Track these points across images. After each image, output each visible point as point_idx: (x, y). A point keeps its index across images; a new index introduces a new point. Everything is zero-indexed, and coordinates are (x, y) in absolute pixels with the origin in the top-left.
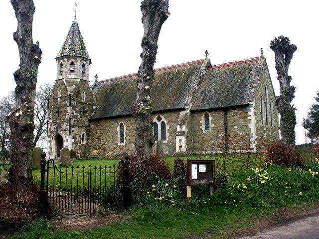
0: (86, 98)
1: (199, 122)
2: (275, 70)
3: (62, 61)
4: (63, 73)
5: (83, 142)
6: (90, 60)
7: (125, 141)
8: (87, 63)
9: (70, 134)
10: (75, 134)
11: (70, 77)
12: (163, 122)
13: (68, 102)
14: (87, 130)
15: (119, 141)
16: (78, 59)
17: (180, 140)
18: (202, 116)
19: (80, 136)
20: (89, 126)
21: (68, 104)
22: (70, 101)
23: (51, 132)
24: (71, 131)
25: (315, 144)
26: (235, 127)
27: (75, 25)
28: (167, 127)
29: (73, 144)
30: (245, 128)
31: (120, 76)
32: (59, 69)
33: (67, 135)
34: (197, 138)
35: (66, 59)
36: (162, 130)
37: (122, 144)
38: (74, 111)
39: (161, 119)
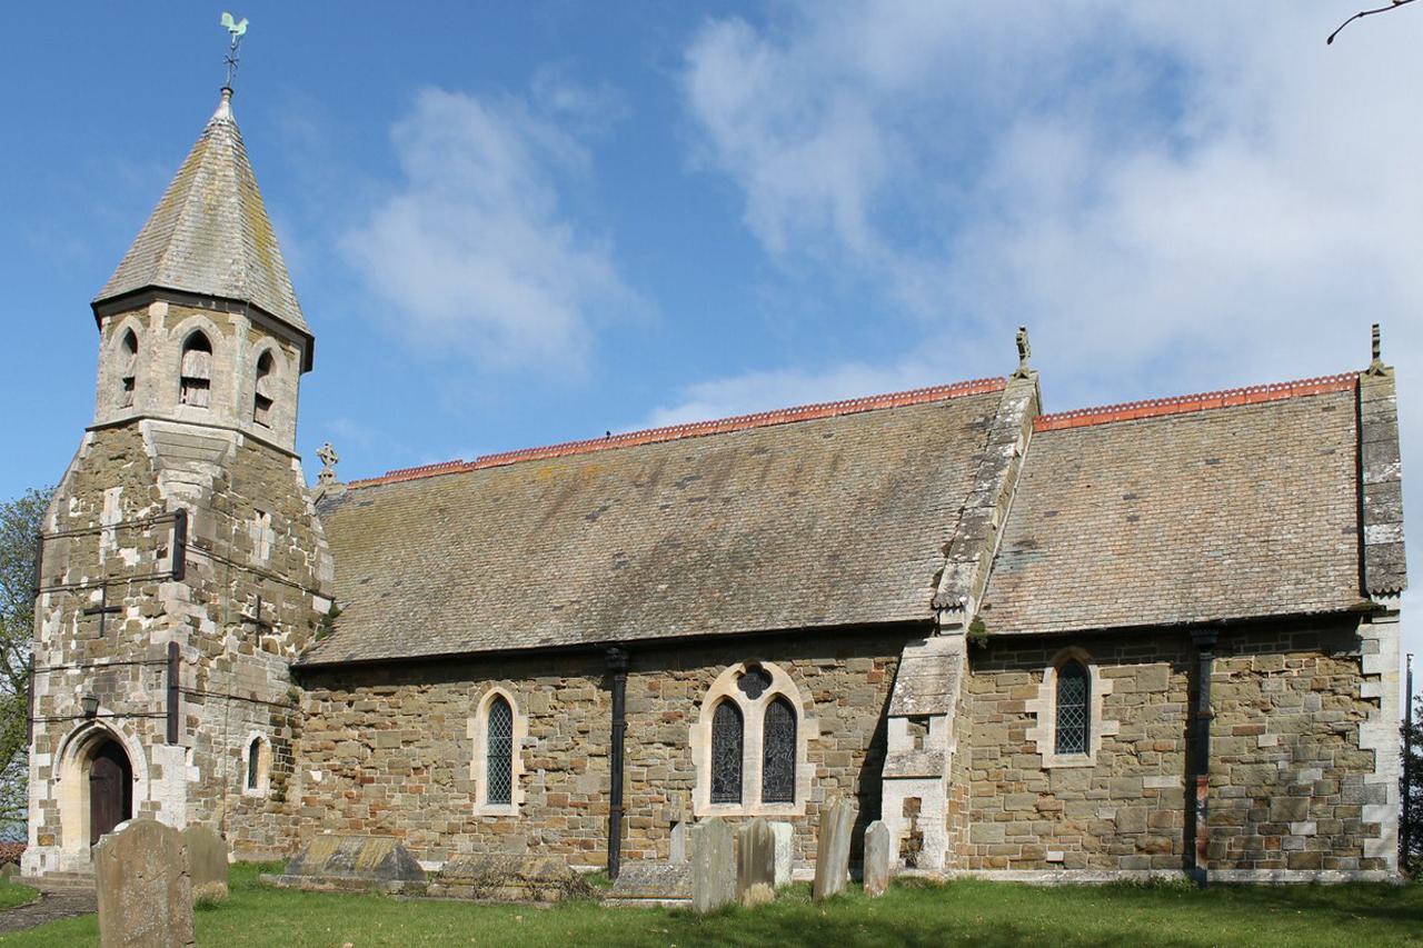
2: (100, 908)
3: (130, 321)
5: (252, 784)
6: (310, 340)
7: (518, 795)
10: (205, 739)
12: (780, 700)
13: (162, 554)
19: (236, 752)
21: (166, 565)
22: (181, 548)
25: (1338, 888)
28: (807, 730)
29: (194, 793)
30: (1334, 747)
33: (158, 740)
35: (159, 309)
37: (499, 809)
38: (200, 612)
39: (767, 679)
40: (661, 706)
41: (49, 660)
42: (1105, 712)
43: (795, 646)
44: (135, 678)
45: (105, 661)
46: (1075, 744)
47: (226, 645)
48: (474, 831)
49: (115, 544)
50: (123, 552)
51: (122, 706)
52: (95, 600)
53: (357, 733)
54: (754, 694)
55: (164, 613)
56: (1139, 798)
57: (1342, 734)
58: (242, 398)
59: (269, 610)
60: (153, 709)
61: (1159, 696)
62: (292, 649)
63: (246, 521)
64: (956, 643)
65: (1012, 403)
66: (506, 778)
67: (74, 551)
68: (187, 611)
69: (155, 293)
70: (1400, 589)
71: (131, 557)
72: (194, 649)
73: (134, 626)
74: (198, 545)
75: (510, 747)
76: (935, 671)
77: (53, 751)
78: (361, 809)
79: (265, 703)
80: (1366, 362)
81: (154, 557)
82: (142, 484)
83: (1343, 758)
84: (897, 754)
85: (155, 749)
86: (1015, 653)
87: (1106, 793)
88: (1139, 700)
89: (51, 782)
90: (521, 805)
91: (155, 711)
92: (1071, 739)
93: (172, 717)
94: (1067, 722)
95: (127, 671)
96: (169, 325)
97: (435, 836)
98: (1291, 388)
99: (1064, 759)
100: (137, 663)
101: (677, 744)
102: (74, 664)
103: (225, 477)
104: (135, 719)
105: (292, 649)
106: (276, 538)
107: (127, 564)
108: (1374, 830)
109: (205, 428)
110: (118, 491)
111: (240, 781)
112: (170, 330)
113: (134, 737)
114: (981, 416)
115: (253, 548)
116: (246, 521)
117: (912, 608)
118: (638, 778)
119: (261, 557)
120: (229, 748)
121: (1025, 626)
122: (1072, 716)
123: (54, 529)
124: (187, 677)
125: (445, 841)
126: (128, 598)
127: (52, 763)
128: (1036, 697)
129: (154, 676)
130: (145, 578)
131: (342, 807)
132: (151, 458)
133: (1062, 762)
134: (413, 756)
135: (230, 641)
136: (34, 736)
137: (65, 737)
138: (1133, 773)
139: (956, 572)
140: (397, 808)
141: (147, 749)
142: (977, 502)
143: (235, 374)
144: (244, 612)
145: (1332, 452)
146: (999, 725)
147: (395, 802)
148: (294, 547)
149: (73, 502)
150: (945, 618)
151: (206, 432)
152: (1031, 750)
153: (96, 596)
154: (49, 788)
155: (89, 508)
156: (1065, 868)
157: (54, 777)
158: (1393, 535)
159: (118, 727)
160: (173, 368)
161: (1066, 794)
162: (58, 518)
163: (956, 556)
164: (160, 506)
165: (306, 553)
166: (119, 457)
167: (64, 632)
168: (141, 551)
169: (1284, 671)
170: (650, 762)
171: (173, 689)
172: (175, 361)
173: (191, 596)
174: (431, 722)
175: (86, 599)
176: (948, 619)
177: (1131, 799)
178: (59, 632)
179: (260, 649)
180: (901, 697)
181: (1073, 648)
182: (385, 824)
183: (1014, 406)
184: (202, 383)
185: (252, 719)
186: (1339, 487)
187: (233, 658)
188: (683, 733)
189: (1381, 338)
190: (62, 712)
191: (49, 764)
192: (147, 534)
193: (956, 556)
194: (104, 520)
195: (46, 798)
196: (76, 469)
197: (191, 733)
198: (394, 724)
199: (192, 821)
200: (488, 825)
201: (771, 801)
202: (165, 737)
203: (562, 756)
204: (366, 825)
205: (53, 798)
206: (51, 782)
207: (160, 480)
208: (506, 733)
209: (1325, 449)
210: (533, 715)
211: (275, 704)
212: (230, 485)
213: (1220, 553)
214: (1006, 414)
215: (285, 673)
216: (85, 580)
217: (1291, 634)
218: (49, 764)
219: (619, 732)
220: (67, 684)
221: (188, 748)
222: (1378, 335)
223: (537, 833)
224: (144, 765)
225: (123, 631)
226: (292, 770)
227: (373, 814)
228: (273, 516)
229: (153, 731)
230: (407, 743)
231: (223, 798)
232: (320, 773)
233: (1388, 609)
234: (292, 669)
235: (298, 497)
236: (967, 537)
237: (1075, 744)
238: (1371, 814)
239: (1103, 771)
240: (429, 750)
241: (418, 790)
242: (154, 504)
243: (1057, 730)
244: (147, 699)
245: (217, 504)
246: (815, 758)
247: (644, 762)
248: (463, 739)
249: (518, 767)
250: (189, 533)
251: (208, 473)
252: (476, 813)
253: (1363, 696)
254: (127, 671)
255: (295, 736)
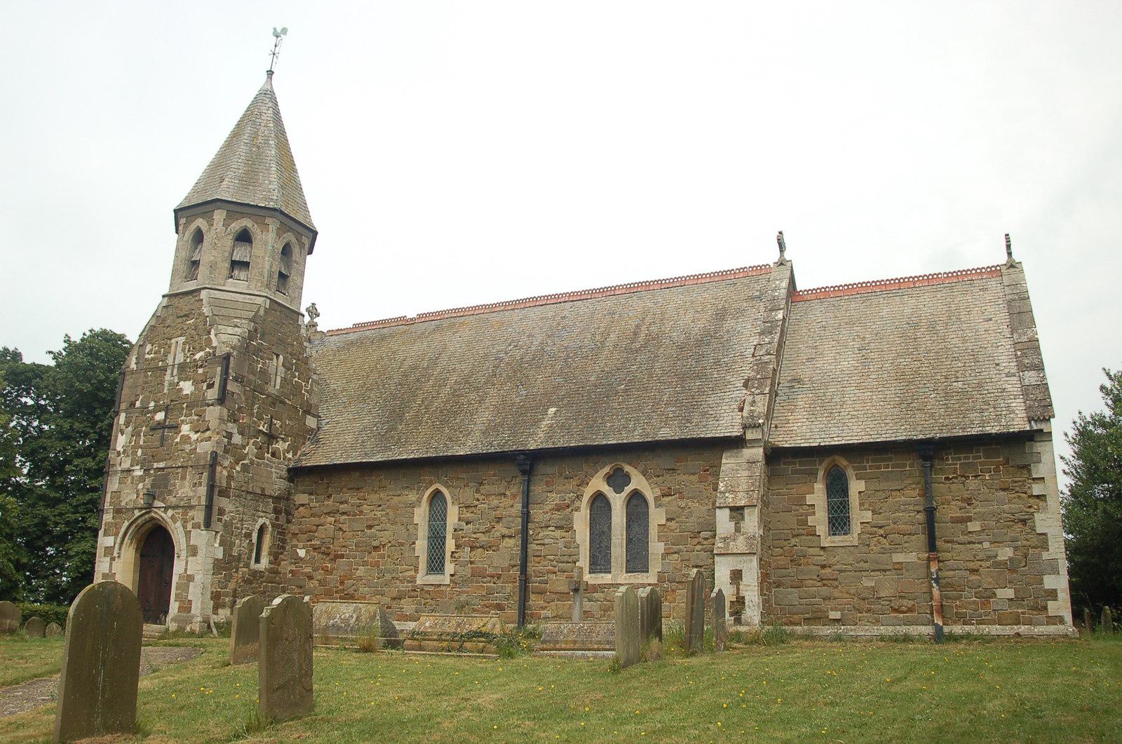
0: (284, 379)
1: (800, 501)
3: (200, 223)
4: (203, 270)
5: (258, 561)
6: (315, 233)
7: (449, 568)
8: (302, 245)
9: (208, 524)
11: (230, 284)
12: (636, 496)
13: (210, 386)
14: (277, 511)
15: (423, 565)
16: (268, 220)
17: (736, 576)
18: (813, 474)
19: (248, 535)
20: (286, 497)
21: (212, 394)
23: (118, 511)
24: (215, 510)
26: (974, 526)
27: (267, 97)
28: (657, 517)
29: (218, 566)
31: (411, 314)
32: (184, 254)
33: (197, 526)
34: (792, 570)
35: (219, 216)
36: (628, 527)
37: (434, 579)
38: (233, 428)
40: (554, 499)
41: (120, 465)
42: (861, 504)
43: (647, 454)
44: (183, 478)
45: (162, 465)
46: (842, 528)
47: (247, 454)
48: (417, 597)
49: (176, 378)
50: (182, 383)
51: (172, 500)
52: (158, 419)
53: (333, 519)
54: (618, 490)
55: (208, 429)
56: (890, 570)
57: (1024, 522)
58: (270, 276)
59: (277, 426)
60: (193, 502)
61: (898, 493)
62: (290, 456)
63: (267, 361)
64: (758, 453)
65: (777, 282)
66: (441, 555)
67: (146, 383)
68: (224, 427)
69: (219, 203)
70: (1050, 417)
71: (187, 387)
72: (227, 456)
73: (186, 439)
74: (236, 379)
75: (445, 530)
76: (746, 473)
77: (116, 535)
78: (334, 578)
79: (270, 496)
80: (1003, 259)
81: (205, 388)
82: (198, 337)
83: (1026, 540)
84: (723, 536)
85: (194, 533)
86: (797, 460)
87: (866, 566)
88: (884, 495)
89: (113, 559)
90: (452, 575)
91: (197, 503)
92: (839, 524)
93: (209, 508)
94: (836, 511)
95: (178, 473)
96: (226, 225)
97: (386, 600)
98: (957, 275)
99: (836, 540)
100: (186, 467)
101: (567, 527)
102: (138, 467)
103: (256, 330)
104: (180, 510)
105: (290, 456)
106: (286, 372)
107: (185, 393)
108: (1053, 594)
109: (245, 296)
110: (182, 340)
111: (249, 558)
112: (227, 228)
113: (179, 524)
114: (757, 291)
115: (270, 381)
116: (267, 361)
117: (728, 425)
118: (538, 554)
119: (275, 387)
120: (244, 531)
121: (803, 441)
122: (838, 507)
123: (133, 366)
124: (222, 473)
125: (394, 604)
126: (182, 418)
127: (115, 544)
128: (814, 493)
129: (197, 476)
130: (196, 403)
131: (319, 577)
132: (207, 317)
133: (835, 542)
134: (374, 537)
135: (250, 449)
136: (103, 523)
137: (126, 524)
138: (884, 551)
139: (754, 402)
140: (361, 578)
141: (188, 534)
142: (762, 352)
143: (267, 258)
144: (261, 428)
145: (991, 319)
146: (789, 513)
147: (358, 573)
148: (296, 379)
149: (149, 347)
150: (750, 435)
151: (245, 299)
152: (813, 533)
153: (160, 416)
154: (111, 564)
155: (160, 352)
156: (843, 625)
157: (115, 555)
158: (1039, 378)
159: (166, 517)
160: (227, 254)
161: (838, 567)
162: (136, 358)
163: (753, 390)
164: (211, 351)
165: (303, 384)
166: (185, 316)
167: (133, 444)
168: (195, 383)
169: (980, 475)
170: (546, 541)
171: (211, 488)
172: (229, 249)
173: (228, 416)
174: (388, 511)
175: (152, 418)
176: (751, 435)
177: (885, 571)
178: (130, 443)
179: (269, 455)
180: (724, 493)
181: (836, 457)
182: (351, 591)
183: (779, 284)
184: (245, 265)
185: (260, 509)
186: (999, 344)
187: (252, 462)
188: (569, 519)
189: (1012, 243)
190: (127, 504)
191: (112, 545)
192: (200, 371)
193: (753, 390)
194: (170, 361)
195: (108, 572)
196: (153, 324)
197: (220, 520)
198: (361, 512)
199: (215, 590)
200: (428, 592)
201: (632, 572)
202: (202, 524)
203: (483, 538)
204: (336, 592)
205: (113, 572)
206: (113, 559)
207: (213, 332)
208: (442, 519)
209: (986, 317)
210: (461, 505)
211: (276, 497)
212: (259, 336)
213: (927, 390)
214: (774, 290)
215: (284, 473)
216: (152, 404)
217: (981, 448)
218: (112, 545)
219: (526, 517)
220: (132, 483)
221: (217, 532)
222: (1009, 241)
223: (463, 598)
224: (184, 546)
225: (177, 443)
226: (284, 548)
227: (342, 583)
228: (284, 357)
229: (193, 519)
230: (370, 527)
231: (237, 572)
232: (304, 551)
233: (1044, 431)
234: (289, 470)
235: (301, 344)
236: (759, 376)
237: (842, 528)
238: (1049, 582)
239: (865, 549)
240: (386, 532)
241: (377, 564)
242: (208, 350)
243: (829, 518)
244: (191, 494)
245: (247, 348)
246: (664, 539)
247: (542, 542)
248: (409, 525)
249: (450, 545)
250: (230, 371)
251: (244, 328)
252: (419, 582)
253: (1034, 494)
254: (178, 473)
255: (289, 521)
